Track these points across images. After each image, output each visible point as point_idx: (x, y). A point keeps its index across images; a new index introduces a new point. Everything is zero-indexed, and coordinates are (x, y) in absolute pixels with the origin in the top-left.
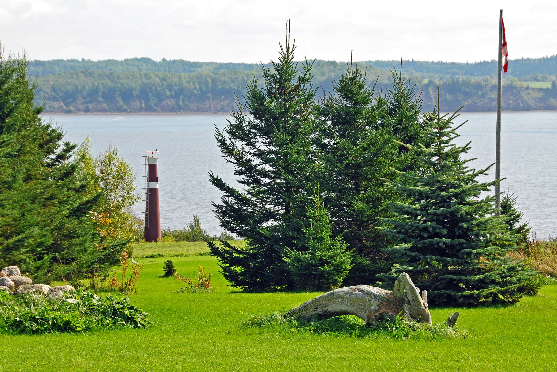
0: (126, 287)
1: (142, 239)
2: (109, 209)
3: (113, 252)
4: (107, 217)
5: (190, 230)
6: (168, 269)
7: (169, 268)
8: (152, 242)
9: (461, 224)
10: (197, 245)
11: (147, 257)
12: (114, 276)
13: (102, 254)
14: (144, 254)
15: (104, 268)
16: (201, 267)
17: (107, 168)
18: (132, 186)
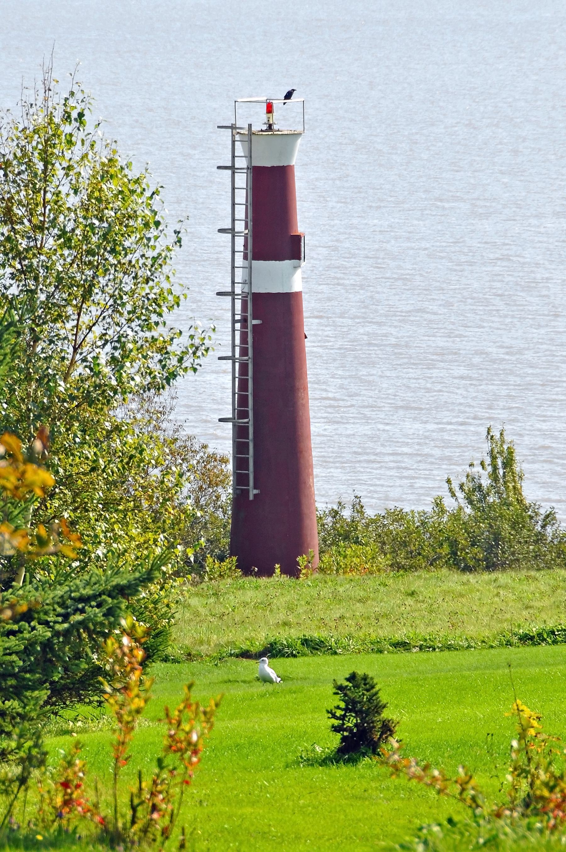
0: (133, 822)
1: (221, 559)
2: (45, 409)
3: (67, 633)
4: (31, 457)
5: (468, 510)
6: (351, 722)
7: (358, 713)
8: (270, 573)
9: (100, 679)
10: (505, 587)
11: (245, 655)
12: (70, 764)
13: (12, 642)
14: (230, 636)
15: (23, 717)
16: (527, 712)
17: (36, 191)
18: (165, 285)
